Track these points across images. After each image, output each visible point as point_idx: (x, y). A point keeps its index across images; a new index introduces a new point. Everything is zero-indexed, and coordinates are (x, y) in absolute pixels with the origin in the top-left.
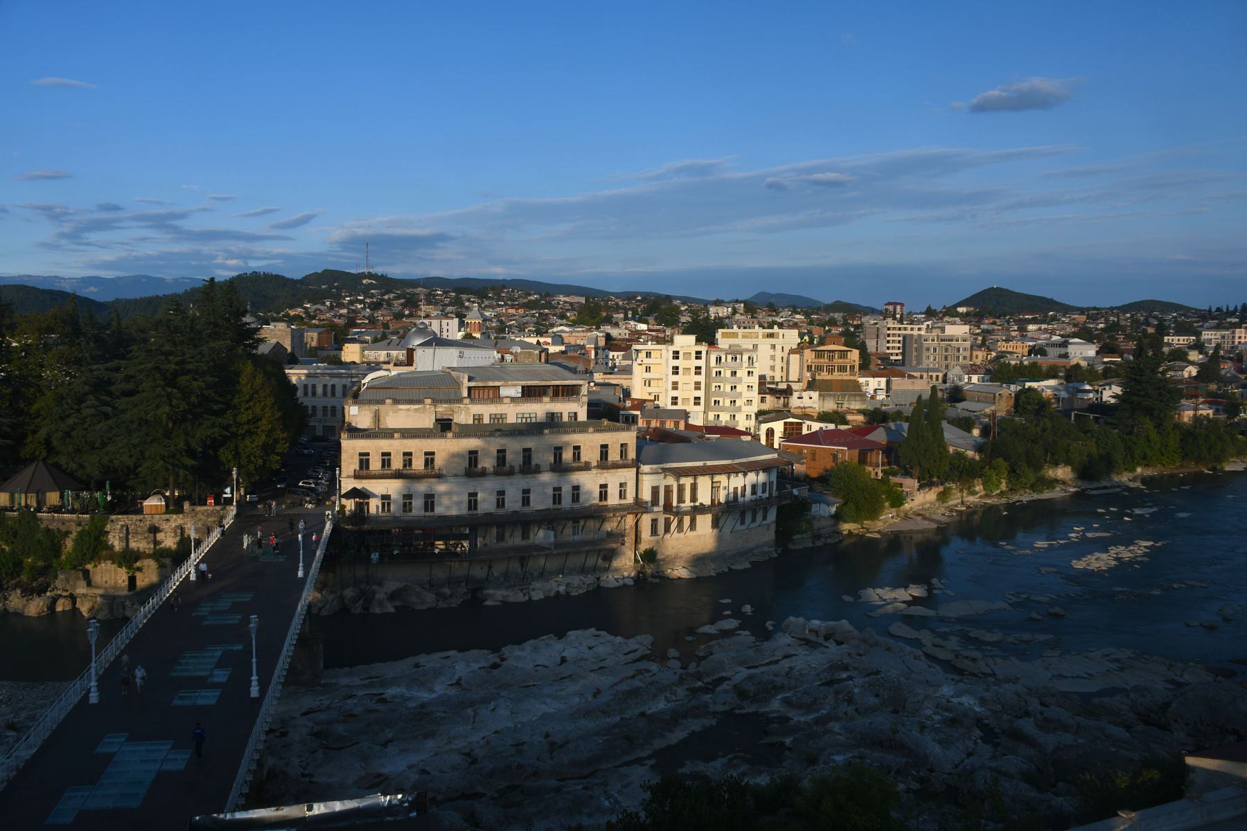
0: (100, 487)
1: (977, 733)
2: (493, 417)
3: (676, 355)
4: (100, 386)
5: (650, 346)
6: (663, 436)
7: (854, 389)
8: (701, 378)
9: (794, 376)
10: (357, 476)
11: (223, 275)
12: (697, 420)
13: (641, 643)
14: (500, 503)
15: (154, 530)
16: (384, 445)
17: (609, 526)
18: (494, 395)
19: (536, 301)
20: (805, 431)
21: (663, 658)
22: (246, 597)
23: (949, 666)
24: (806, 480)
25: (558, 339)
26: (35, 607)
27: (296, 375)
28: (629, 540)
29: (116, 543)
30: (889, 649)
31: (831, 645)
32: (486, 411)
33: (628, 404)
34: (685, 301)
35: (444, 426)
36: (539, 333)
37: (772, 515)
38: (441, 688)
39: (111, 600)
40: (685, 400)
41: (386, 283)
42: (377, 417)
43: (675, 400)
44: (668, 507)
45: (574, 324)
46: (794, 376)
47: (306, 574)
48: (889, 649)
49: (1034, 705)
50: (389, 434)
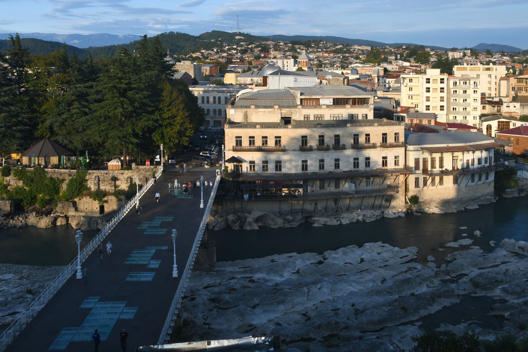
0: (82, 154)
2: (316, 116)
4: (81, 97)
5: (412, 75)
6: (421, 129)
8: (444, 95)
9: (503, 93)
10: (234, 150)
11: (152, 33)
12: (442, 118)
13: (411, 251)
14: (322, 167)
15: (115, 179)
16: (251, 132)
17: (388, 182)
18: (316, 103)
19: (342, 49)
20: (511, 127)
21: (423, 260)
22: (170, 219)
24: (513, 156)
25: (355, 71)
26: (44, 223)
27: (197, 91)
28: (402, 190)
29: (92, 185)
32: (312, 113)
33: (399, 109)
34: (433, 48)
35: (286, 121)
36: (343, 67)
37: (492, 177)
38: (287, 275)
39: (90, 219)
41: (250, 38)
42: (246, 116)
43: (428, 108)
44: (425, 171)
45: (364, 62)
46: (503, 93)
47: (205, 206)
50: (253, 125)
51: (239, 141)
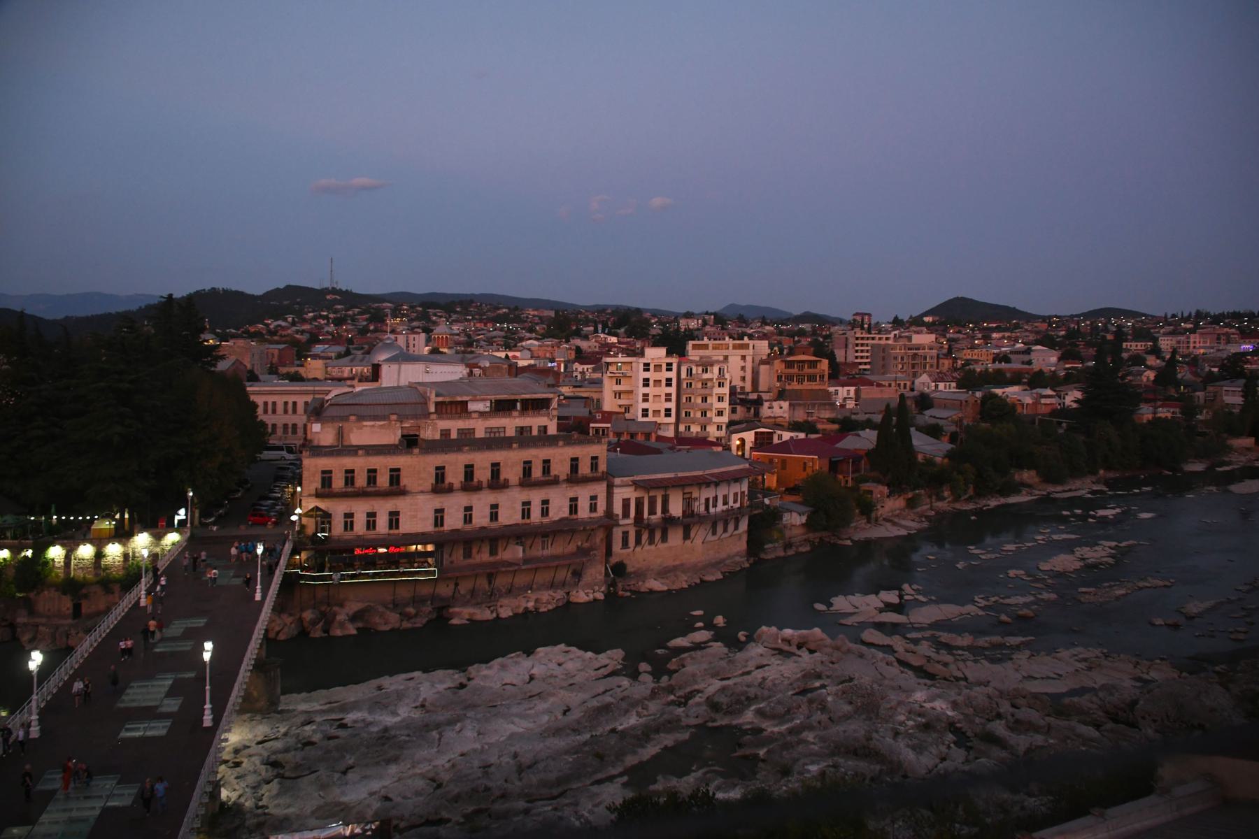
1: (950, 737)
3: (646, 367)
7: (826, 399)
10: (318, 495)
16: (348, 462)
18: (461, 409)
21: (635, 675)
23: (920, 672)
30: (861, 656)
31: (804, 654)
32: (454, 426)
34: (655, 313)
35: (410, 442)
36: (508, 347)
37: (744, 525)
40: (656, 412)
41: (349, 298)
43: (645, 411)
46: (763, 386)
48: (861, 656)
49: (1005, 707)
50: (353, 450)
51: (327, 478)
